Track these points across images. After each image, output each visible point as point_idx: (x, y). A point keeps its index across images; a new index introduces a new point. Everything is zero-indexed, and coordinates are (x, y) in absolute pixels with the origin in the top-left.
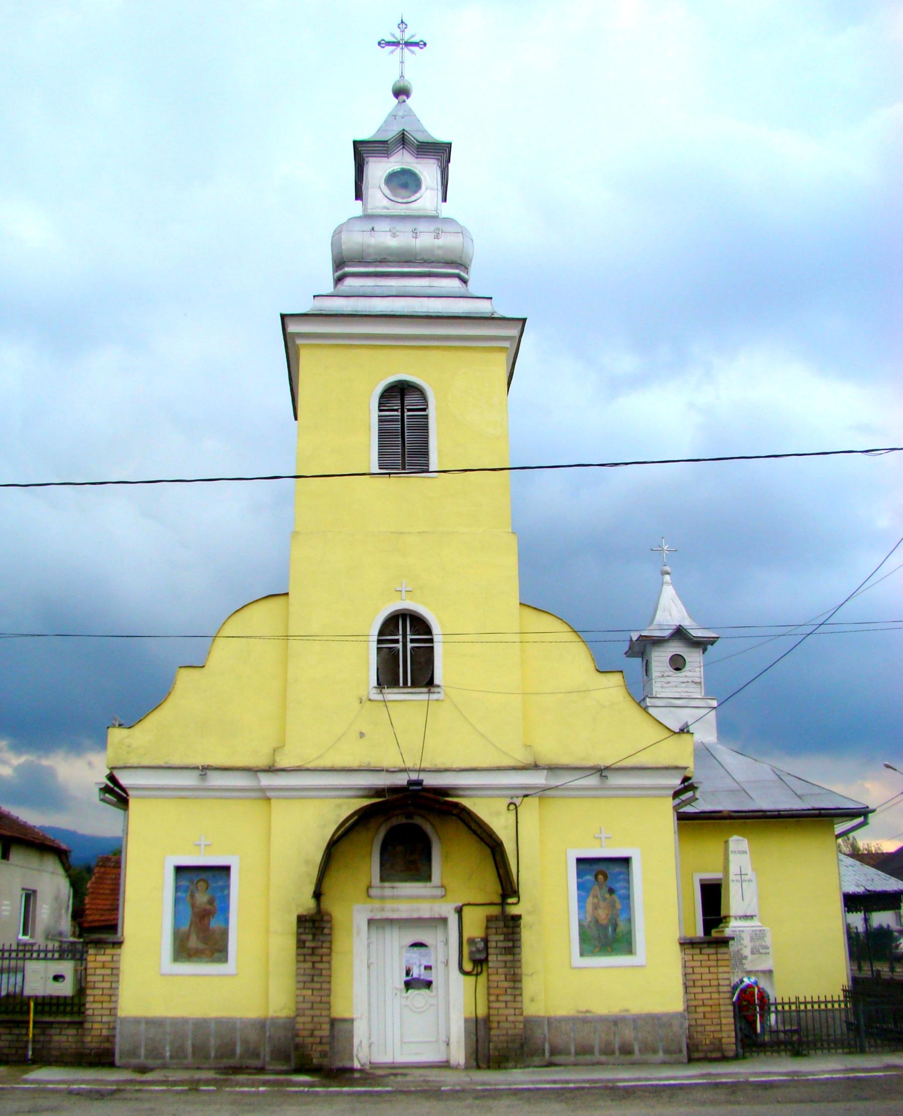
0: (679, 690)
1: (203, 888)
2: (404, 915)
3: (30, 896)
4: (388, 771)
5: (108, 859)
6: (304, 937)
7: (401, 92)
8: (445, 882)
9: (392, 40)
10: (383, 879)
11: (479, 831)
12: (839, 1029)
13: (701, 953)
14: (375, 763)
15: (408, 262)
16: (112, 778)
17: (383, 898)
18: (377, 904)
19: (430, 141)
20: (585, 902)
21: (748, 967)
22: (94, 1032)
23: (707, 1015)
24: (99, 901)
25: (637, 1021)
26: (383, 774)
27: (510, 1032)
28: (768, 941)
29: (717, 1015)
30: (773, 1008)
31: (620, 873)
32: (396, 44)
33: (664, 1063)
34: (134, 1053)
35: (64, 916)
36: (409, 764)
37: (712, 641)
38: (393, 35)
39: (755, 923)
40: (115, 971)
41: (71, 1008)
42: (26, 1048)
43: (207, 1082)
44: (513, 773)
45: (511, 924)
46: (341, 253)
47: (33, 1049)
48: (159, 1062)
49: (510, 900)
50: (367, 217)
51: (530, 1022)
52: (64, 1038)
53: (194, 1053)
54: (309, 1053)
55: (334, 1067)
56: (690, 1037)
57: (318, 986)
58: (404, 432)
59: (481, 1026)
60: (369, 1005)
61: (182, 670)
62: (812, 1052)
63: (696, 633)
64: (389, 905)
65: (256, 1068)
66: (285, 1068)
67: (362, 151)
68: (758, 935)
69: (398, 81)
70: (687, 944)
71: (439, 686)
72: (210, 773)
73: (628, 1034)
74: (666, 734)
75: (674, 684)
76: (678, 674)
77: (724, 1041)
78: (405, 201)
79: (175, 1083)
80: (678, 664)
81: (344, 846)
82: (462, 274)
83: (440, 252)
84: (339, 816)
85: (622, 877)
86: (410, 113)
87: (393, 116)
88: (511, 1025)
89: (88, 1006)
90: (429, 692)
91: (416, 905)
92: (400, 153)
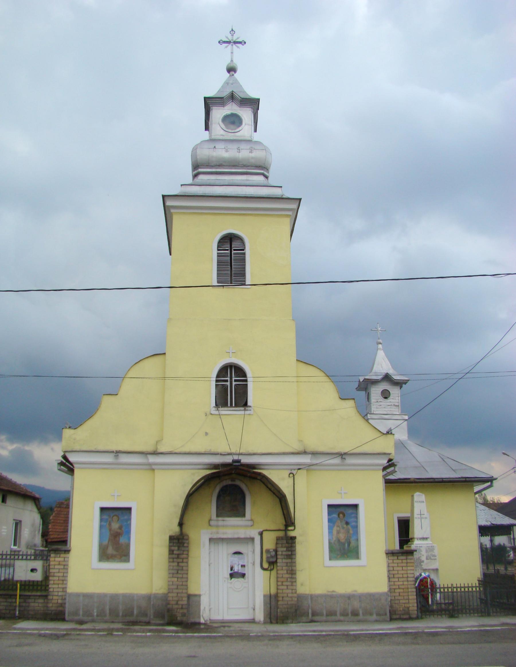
0: (386, 409)
1: (116, 520)
2: (230, 536)
3: (18, 524)
4: (221, 454)
5: (62, 503)
6: (173, 548)
7: (231, 70)
10: (218, 516)
11: (272, 489)
13: (398, 559)
14: (214, 450)
15: (235, 166)
16: (65, 457)
17: (217, 526)
18: (214, 530)
22: (53, 601)
25: (361, 597)
26: (218, 456)
27: (289, 603)
28: (436, 552)
29: (406, 594)
30: (438, 590)
31: (352, 513)
32: (229, 42)
33: (376, 621)
34: (76, 613)
36: (233, 451)
37: (405, 382)
38: (227, 37)
39: (429, 542)
40: (66, 567)
41: (41, 588)
42: (15, 610)
43: (118, 630)
44: (292, 456)
45: (290, 541)
47: (19, 611)
48: (90, 618)
49: (290, 528)
51: (301, 597)
52: (37, 604)
54: (174, 614)
55: (189, 622)
56: (391, 606)
57: (180, 576)
58: (232, 261)
59: (273, 600)
60: (210, 587)
62: (460, 615)
63: (396, 377)
64: (221, 530)
65: (145, 622)
66: (162, 622)
68: (430, 549)
70: (390, 554)
71: (250, 407)
73: (356, 604)
74: (380, 434)
75: (383, 406)
76: (386, 400)
77: (410, 609)
78: (233, 131)
79: (99, 630)
80: (386, 395)
82: (266, 173)
83: (253, 161)
85: (353, 515)
86: (236, 82)
87: (227, 83)
88: (290, 599)
89: (50, 586)
90: (245, 410)
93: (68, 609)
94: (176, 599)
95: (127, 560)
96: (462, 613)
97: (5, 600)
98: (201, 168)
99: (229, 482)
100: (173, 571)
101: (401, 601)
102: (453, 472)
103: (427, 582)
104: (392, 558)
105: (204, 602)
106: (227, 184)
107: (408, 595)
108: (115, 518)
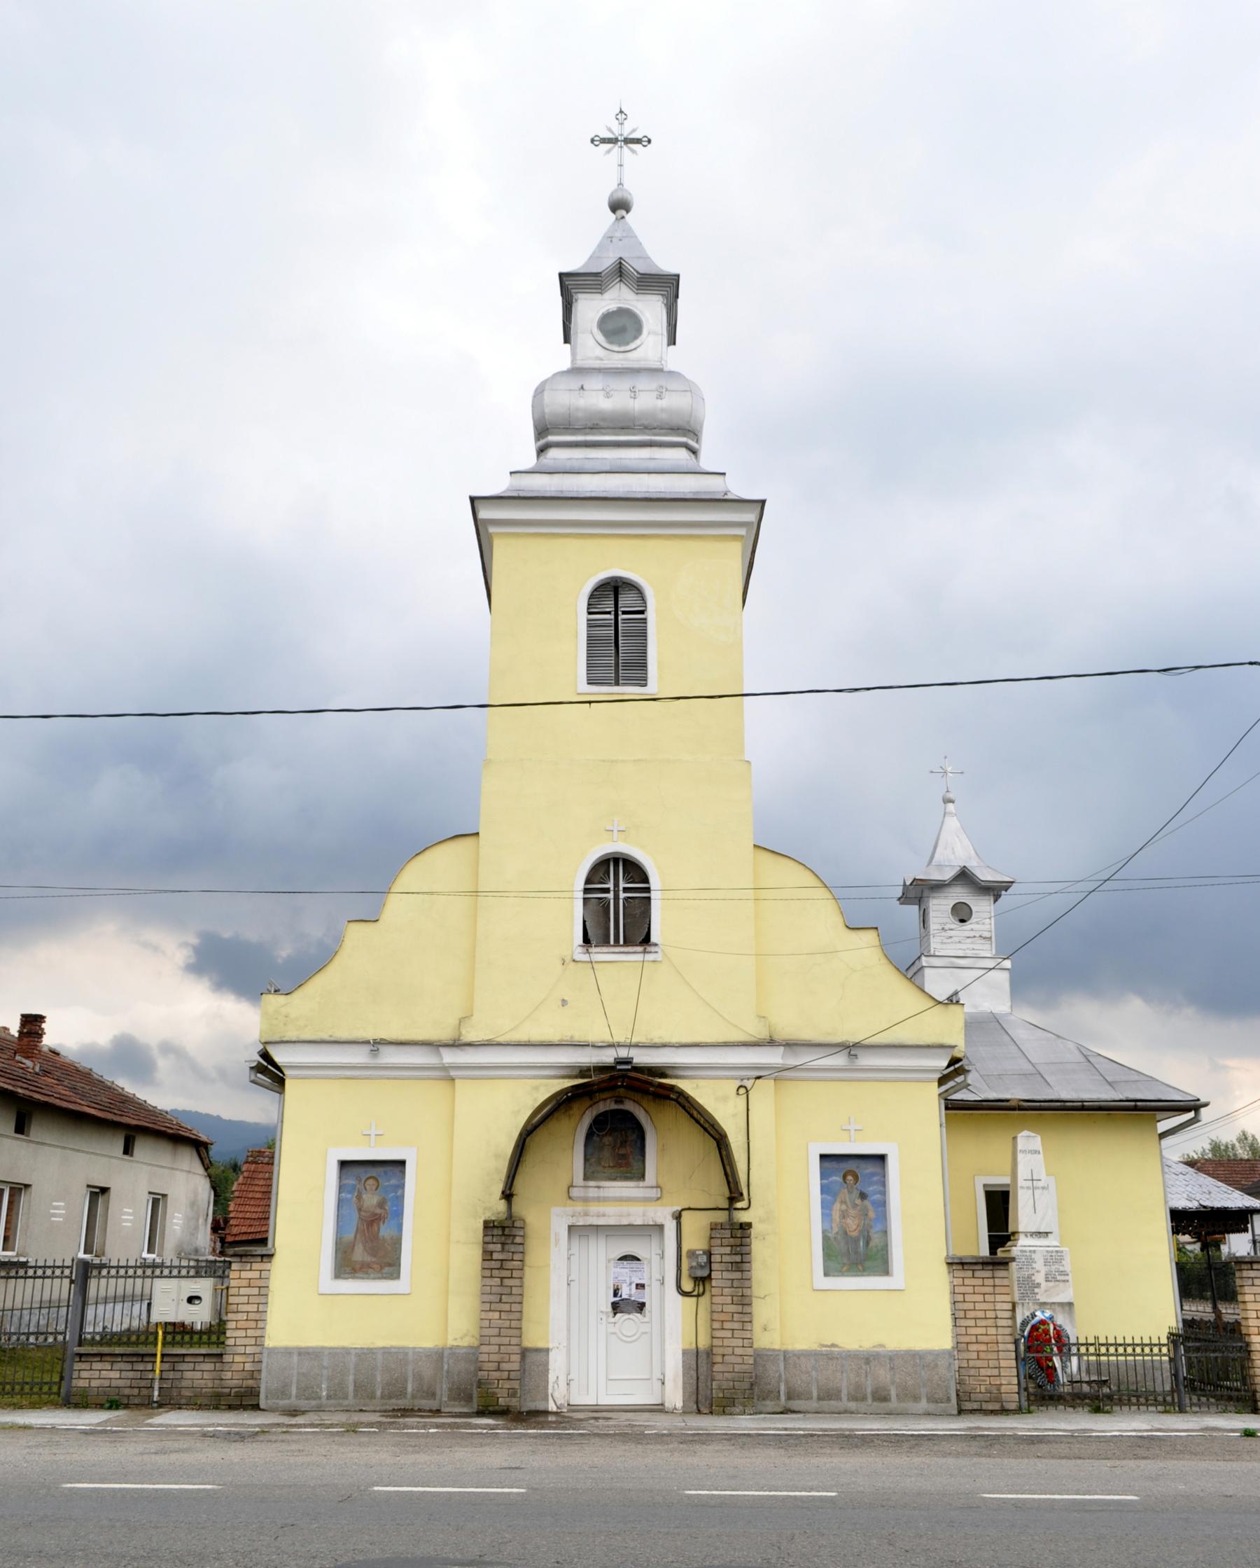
0: (964, 946)
1: (372, 1186)
2: (612, 1222)
3: (158, 1202)
4: (593, 1046)
5: (260, 1153)
6: (491, 1247)
7: (619, 206)
9: (610, 136)
10: (586, 1178)
11: (702, 1121)
12: (1164, 1383)
14: (579, 1036)
15: (624, 429)
16: (265, 1055)
17: (586, 1200)
18: (579, 1208)
19: (653, 272)
22: (235, 1367)
23: (982, 1355)
24: (247, 1208)
25: (894, 1359)
26: (589, 1050)
27: (737, 1368)
28: (1067, 1265)
29: (994, 1356)
30: (1074, 1350)
31: (873, 1174)
32: (613, 141)
33: (928, 1414)
34: (283, 1392)
35: (201, 1228)
36: (620, 1037)
37: (1006, 886)
38: (610, 130)
39: (1051, 1241)
40: (263, 1291)
42: (152, 1387)
43: (370, 1425)
44: (743, 1049)
45: (739, 1233)
46: (543, 413)
48: (313, 1403)
49: (739, 1205)
50: (576, 371)
51: (761, 1357)
52: (198, 1375)
53: (356, 1391)
54: (494, 1392)
55: (524, 1409)
56: (960, 1383)
57: (507, 1307)
58: (617, 630)
59: (703, 1359)
60: (569, 1331)
61: (353, 926)
62: (1116, 1408)
63: (985, 875)
64: (594, 1208)
65: (430, 1411)
66: (465, 1410)
67: (571, 285)
68: (1055, 1258)
69: (616, 191)
70: (958, 1264)
71: (656, 945)
72: (383, 1049)
73: (883, 1375)
74: (932, 1003)
75: (957, 939)
76: (967, 926)
77: (1003, 1389)
78: (622, 349)
79: (331, 1426)
80: (962, 914)
81: (541, 1134)
82: (692, 443)
83: (664, 416)
84: (535, 1100)
85: (875, 1178)
86: (630, 234)
87: (609, 238)
88: (739, 1360)
89: (229, 1334)
90: (645, 952)
91: (624, 1208)
92: (617, 289)
93: (266, 1384)
94: (494, 1357)
95: (395, 1275)
96: (1121, 1403)
97: (129, 1367)
98: (552, 434)
99: (614, 1106)
100: (492, 1298)
101: (983, 1372)
102: (1108, 1087)
103: (1046, 1332)
105: (557, 1366)
106: (607, 468)
108: (371, 1182)
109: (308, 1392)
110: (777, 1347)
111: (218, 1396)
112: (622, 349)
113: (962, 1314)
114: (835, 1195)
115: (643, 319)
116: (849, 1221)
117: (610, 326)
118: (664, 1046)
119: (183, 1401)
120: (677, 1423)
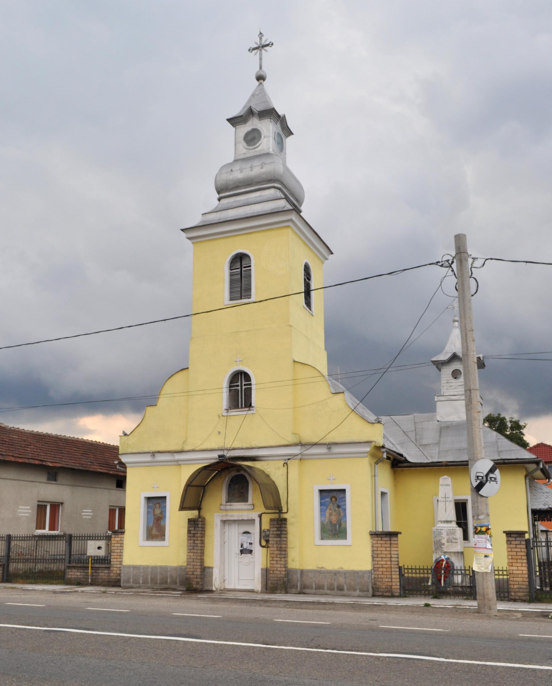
0: (458, 390)
2: (236, 519)
6: (191, 529)
7: (260, 78)
8: (254, 503)
13: (381, 540)
17: (226, 510)
18: (224, 513)
20: (325, 512)
21: (445, 550)
22: (114, 572)
23: (384, 573)
25: (345, 574)
27: (278, 576)
34: (128, 581)
41: (105, 561)
44: (283, 448)
47: (92, 579)
48: (138, 585)
52: (103, 574)
54: (193, 582)
57: (195, 551)
64: (230, 513)
72: (156, 455)
73: (341, 580)
75: (455, 387)
77: (393, 587)
78: (254, 147)
83: (264, 176)
88: (279, 572)
90: (249, 410)
91: (241, 513)
95: (164, 540)
97: (82, 571)
101: (384, 580)
104: (376, 539)
105: (216, 573)
107: (391, 575)
108: (158, 505)
109: (136, 581)
110: (297, 568)
111: (109, 582)
112: (254, 147)
113: (376, 556)
114: (327, 507)
115: (262, 131)
116: (333, 517)
117: (250, 137)
118: (253, 448)
119: (517, 598)
120: (259, 597)
